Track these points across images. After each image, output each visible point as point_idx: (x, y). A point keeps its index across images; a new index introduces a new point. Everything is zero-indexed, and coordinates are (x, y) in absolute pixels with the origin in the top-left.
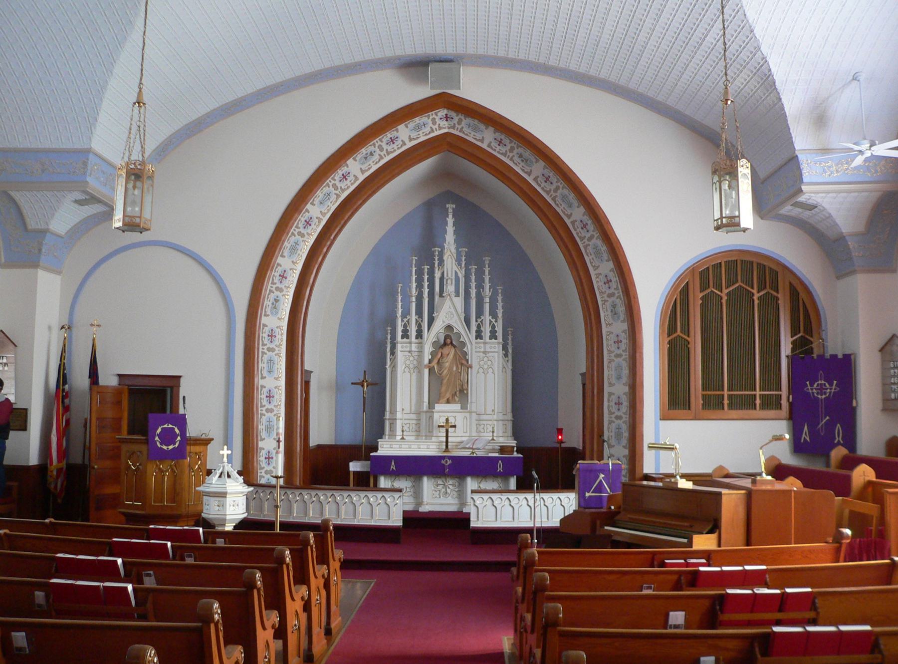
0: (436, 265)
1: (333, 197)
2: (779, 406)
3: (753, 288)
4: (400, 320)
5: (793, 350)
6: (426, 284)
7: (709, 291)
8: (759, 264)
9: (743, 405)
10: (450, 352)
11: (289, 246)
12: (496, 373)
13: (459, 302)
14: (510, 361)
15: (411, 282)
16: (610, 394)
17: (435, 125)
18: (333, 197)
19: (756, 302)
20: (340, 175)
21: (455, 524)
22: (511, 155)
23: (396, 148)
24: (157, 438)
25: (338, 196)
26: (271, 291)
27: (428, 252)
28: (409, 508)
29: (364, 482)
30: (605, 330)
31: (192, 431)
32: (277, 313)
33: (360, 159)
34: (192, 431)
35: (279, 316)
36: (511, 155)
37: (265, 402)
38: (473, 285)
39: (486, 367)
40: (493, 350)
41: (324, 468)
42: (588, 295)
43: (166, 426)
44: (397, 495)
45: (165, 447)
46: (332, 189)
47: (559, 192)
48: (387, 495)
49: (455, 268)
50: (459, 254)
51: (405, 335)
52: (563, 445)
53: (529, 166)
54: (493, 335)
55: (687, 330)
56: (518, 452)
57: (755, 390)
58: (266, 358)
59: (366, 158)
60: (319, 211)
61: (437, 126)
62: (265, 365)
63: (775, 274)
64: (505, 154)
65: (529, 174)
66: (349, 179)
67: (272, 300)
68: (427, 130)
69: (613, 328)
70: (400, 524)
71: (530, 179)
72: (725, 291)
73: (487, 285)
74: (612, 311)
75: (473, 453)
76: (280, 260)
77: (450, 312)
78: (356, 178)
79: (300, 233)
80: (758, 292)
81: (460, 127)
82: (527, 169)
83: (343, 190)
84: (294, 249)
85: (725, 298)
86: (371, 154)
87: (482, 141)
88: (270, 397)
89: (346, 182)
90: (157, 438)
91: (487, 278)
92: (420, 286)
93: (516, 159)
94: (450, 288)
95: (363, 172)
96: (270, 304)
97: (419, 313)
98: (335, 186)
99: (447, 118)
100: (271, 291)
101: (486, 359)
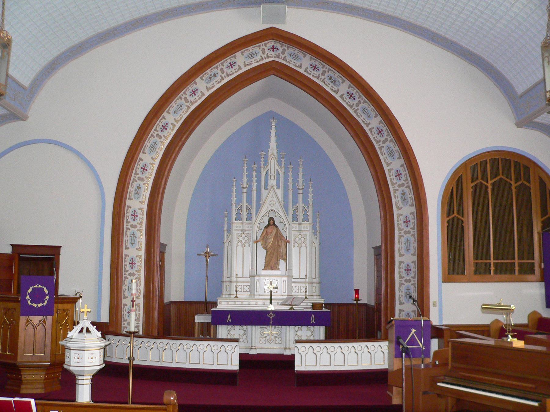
0: (262, 165)
1: (185, 108)
2: (532, 272)
3: (511, 180)
4: (234, 206)
5: (543, 228)
6: (254, 179)
7: (478, 181)
8: (515, 162)
9: (505, 271)
10: (272, 230)
11: (149, 145)
12: (308, 246)
13: (280, 193)
14: (318, 238)
15: (242, 177)
16: (401, 263)
17: (262, 54)
18: (185, 108)
19: (514, 190)
20: (190, 91)
21: (280, 366)
22: (323, 77)
23: (234, 71)
24: (28, 297)
25: (188, 107)
26: (134, 180)
27: (256, 157)
28: (243, 351)
29: (207, 334)
30: (395, 212)
31: (64, 290)
32: (139, 197)
33: (206, 79)
34: (64, 290)
35: (140, 200)
36: (323, 77)
37: (128, 268)
38: (290, 180)
39: (300, 242)
40: (305, 229)
41: (173, 321)
42: (382, 183)
43: (36, 286)
44: (234, 344)
45: (35, 305)
46: (183, 101)
47: (360, 105)
48: (226, 344)
49: (277, 168)
50: (279, 156)
51: (239, 217)
52: (359, 302)
53: (337, 86)
54: (306, 218)
55: (461, 212)
56: (326, 307)
57: (514, 259)
58: (129, 232)
59: (210, 78)
60: (174, 118)
61: (265, 55)
62: (129, 238)
63: (527, 170)
64: (318, 77)
65: (337, 92)
66: (197, 94)
67: (135, 187)
68: (258, 58)
69: (403, 210)
70: (237, 368)
71: (337, 97)
72: (490, 182)
73: (301, 180)
74: (402, 198)
75: (291, 308)
76: (141, 155)
77: (272, 202)
78: (203, 94)
79: (158, 136)
80: (515, 183)
81: (283, 56)
82: (335, 88)
83: (192, 103)
84: (153, 148)
85: (490, 187)
86: (215, 75)
87: (300, 67)
88: (132, 263)
89: (195, 97)
90: (28, 297)
91: (301, 175)
92: (250, 181)
93: (327, 81)
94: (273, 182)
95: (208, 89)
96: (133, 190)
97: (249, 201)
98: (186, 99)
99: (273, 49)
100: (134, 180)
101: (300, 236)
